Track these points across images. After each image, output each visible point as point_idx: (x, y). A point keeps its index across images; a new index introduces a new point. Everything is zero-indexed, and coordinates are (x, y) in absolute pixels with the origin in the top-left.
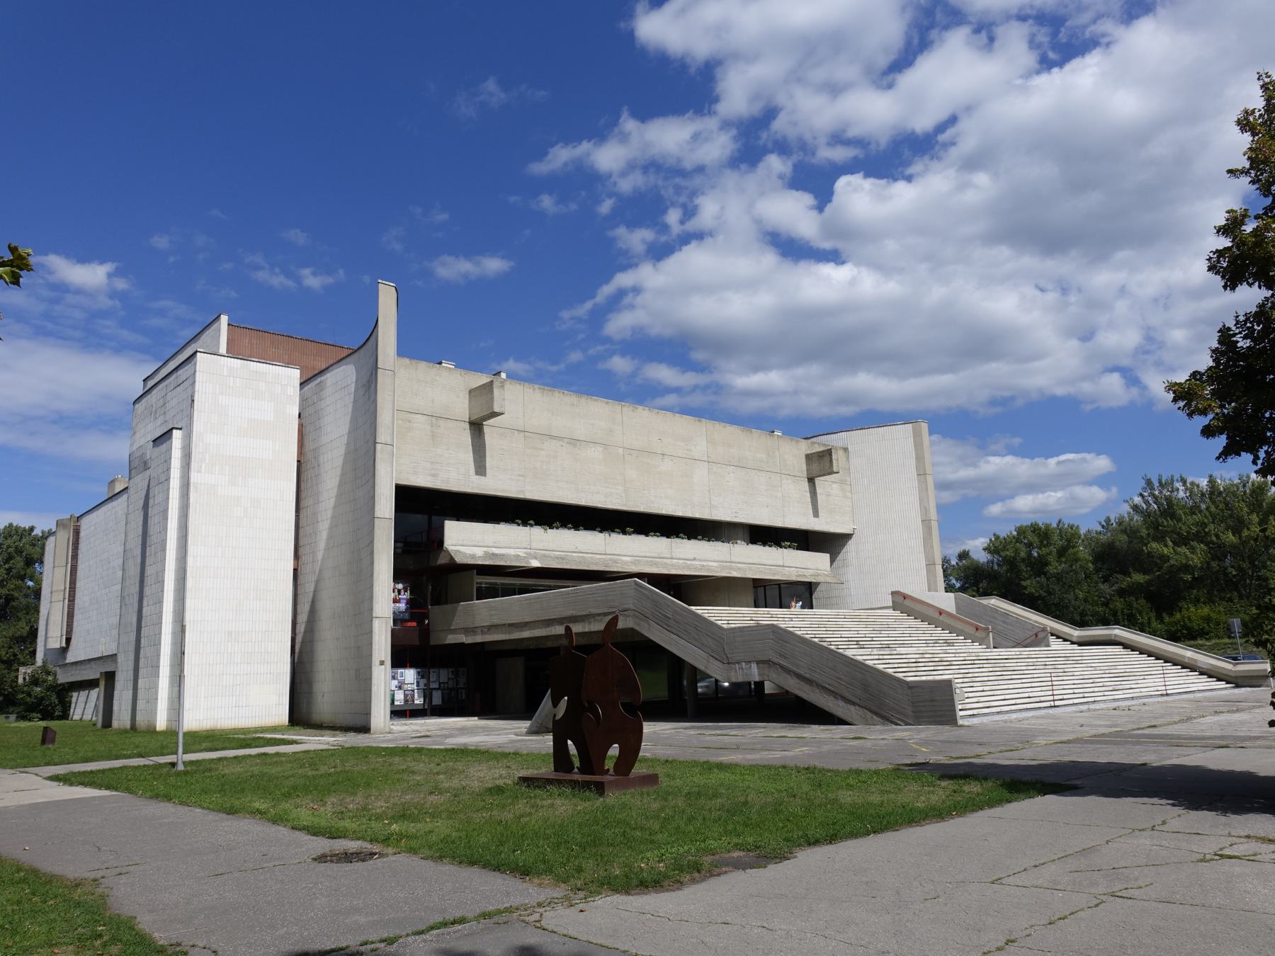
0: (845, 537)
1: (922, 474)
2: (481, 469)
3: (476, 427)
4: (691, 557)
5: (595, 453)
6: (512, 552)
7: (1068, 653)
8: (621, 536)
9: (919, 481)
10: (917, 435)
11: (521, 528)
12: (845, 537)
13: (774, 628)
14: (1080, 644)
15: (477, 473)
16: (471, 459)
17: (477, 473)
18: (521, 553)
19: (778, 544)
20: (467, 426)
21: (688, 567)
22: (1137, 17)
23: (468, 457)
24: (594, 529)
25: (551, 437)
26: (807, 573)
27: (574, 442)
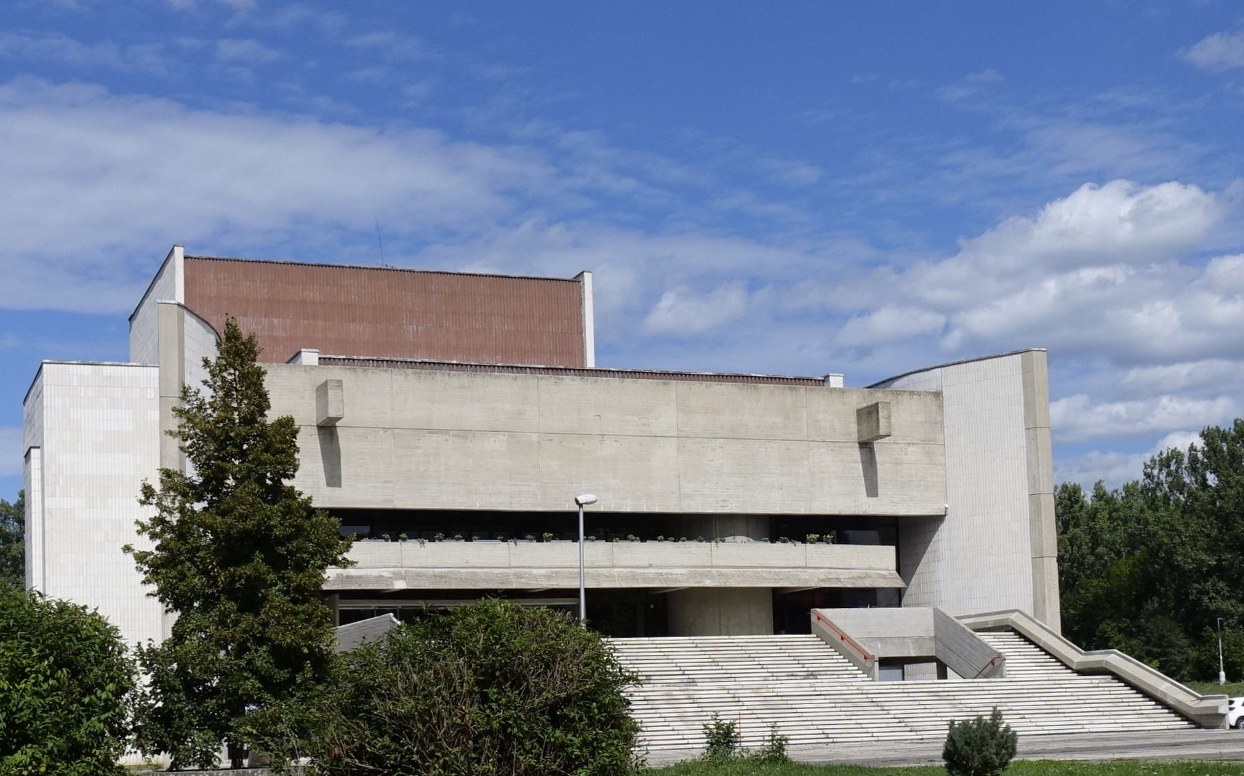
1: (1031, 428)
2: (872, 490)
3: (866, 446)
4: (646, 563)
5: (496, 444)
6: (375, 572)
7: (1066, 684)
8: (535, 544)
9: (1028, 438)
10: (1027, 371)
11: (390, 543)
13: (1087, 648)
14: (1081, 672)
15: (329, 485)
16: (322, 468)
17: (329, 485)
18: (386, 573)
19: (449, 535)
20: (315, 431)
21: (634, 578)
25: (431, 431)
27: (464, 434)
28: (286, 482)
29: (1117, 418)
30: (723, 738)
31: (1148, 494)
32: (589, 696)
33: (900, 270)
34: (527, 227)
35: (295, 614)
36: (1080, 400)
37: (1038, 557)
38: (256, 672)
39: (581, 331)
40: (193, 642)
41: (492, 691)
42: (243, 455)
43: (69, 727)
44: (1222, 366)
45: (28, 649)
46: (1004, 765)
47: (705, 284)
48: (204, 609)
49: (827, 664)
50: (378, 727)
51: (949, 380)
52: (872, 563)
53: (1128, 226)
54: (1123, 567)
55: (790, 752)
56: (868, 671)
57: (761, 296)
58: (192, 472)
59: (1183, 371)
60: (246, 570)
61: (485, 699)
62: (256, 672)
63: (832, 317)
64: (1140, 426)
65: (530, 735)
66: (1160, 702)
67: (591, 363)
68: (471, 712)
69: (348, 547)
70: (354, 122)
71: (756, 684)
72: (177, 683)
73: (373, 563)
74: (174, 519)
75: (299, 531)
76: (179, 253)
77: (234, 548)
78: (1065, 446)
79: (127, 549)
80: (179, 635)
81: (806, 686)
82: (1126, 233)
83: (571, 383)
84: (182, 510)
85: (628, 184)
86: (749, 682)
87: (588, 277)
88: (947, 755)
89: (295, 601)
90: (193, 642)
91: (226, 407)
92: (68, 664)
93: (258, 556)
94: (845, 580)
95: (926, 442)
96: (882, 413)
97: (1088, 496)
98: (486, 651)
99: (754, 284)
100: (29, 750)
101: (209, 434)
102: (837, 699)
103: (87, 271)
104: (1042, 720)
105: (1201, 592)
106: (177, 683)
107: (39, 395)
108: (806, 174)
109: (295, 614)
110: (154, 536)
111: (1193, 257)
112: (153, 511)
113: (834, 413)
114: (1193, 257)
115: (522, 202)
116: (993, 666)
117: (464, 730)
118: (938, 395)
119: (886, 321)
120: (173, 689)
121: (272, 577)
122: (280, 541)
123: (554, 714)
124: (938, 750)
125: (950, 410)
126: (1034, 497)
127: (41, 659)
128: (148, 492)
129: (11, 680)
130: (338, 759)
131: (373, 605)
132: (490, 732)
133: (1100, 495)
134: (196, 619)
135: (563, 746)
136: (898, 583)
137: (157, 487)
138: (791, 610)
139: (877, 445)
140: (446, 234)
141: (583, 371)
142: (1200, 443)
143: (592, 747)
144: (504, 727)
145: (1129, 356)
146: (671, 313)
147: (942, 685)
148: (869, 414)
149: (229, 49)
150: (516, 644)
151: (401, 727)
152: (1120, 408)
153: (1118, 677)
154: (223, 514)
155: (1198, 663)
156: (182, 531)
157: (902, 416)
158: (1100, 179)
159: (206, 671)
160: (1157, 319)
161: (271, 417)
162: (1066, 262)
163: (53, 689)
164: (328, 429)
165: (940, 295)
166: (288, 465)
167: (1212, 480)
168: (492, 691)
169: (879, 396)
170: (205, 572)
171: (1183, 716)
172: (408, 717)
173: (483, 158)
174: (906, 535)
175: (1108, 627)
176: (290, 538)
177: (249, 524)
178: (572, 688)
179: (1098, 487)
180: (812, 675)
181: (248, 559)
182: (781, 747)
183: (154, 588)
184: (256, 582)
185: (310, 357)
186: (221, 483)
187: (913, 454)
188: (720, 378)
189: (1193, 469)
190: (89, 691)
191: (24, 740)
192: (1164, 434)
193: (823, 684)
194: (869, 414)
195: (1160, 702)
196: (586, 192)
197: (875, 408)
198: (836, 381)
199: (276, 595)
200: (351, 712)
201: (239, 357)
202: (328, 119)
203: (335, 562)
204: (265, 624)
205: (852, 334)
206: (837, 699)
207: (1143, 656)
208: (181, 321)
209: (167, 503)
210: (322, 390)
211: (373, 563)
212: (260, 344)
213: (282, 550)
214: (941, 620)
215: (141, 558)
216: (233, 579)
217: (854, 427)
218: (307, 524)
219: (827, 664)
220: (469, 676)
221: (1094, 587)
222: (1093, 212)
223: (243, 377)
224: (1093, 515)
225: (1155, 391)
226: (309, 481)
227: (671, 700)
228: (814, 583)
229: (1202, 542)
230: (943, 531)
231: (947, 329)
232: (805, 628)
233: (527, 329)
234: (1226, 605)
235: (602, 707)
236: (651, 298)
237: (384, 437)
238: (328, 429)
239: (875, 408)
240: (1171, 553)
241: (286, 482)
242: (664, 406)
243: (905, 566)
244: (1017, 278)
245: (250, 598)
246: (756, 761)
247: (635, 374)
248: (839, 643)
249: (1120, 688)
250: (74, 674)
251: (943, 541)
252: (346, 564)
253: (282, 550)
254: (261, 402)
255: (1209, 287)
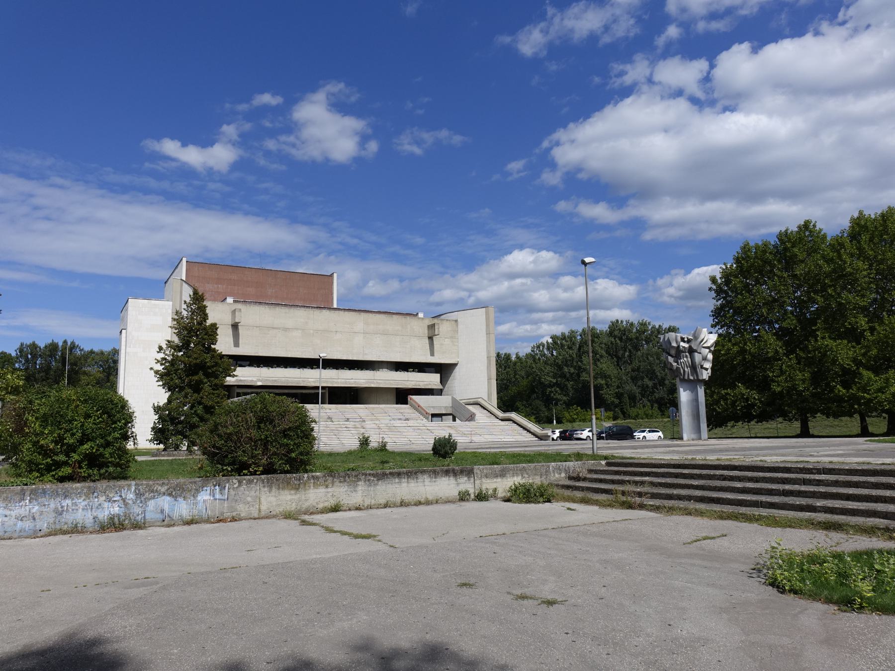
0: (455, 365)
1: (488, 334)
2: (432, 354)
3: (431, 338)
5: (297, 334)
10: (487, 314)
12: (455, 365)
13: (504, 412)
14: (502, 420)
18: (255, 379)
19: (278, 366)
22: (553, 160)
23: (231, 340)
24: (294, 367)
25: (274, 328)
26: (421, 384)
27: (286, 329)
28: (213, 346)
29: (527, 331)
30: (365, 442)
31: (531, 356)
32: (297, 428)
33: (453, 276)
34: (321, 256)
35: (213, 394)
36: (514, 324)
37: (489, 379)
38: (197, 415)
39: (332, 294)
40: (174, 404)
41: (262, 425)
42: (197, 336)
43: (106, 436)
44: (561, 314)
45: (92, 408)
46: (452, 453)
47: (384, 279)
48: (180, 392)
49: (413, 416)
50: (219, 436)
51: (461, 316)
52: (432, 380)
53: (532, 265)
54: (525, 382)
55: (388, 447)
56: (427, 418)
57: (405, 284)
58: (176, 340)
59: (550, 315)
60: (196, 378)
61: (259, 428)
62: (197, 415)
63: (430, 292)
64: (535, 334)
65: (276, 440)
66: (529, 431)
67: (335, 306)
68: (254, 433)
69: (235, 370)
70: (257, 215)
71: (388, 422)
72: (167, 419)
73: (245, 375)
74: (169, 358)
75: (216, 364)
76: (184, 260)
77: (192, 370)
78: (501, 339)
79: (151, 369)
80: (170, 401)
81: (404, 423)
82: (531, 267)
83: (326, 313)
84: (173, 355)
85: (355, 241)
86: (385, 421)
87: (335, 275)
88: (433, 449)
89: (214, 389)
90: (174, 404)
91: (192, 319)
92: (107, 413)
93: (201, 373)
94: (422, 386)
95: (452, 337)
96: (436, 327)
97: (513, 358)
98: (261, 411)
99: (401, 279)
100: (89, 444)
101: (185, 328)
102: (416, 428)
103: (153, 263)
104: (487, 437)
105: (551, 392)
106: (167, 419)
107: (127, 310)
108: (419, 240)
109: (213, 394)
110: (162, 364)
111: (555, 275)
112: (162, 355)
113: (419, 326)
114: (555, 275)
115: (317, 248)
116: (471, 418)
117: (251, 439)
118: (456, 321)
119: (448, 294)
120: (166, 421)
121: (206, 380)
122: (209, 367)
123: (285, 433)
124: (430, 447)
125: (460, 326)
126: (489, 358)
127: (97, 411)
128: (160, 348)
129: (85, 418)
130: (206, 448)
131: (249, 391)
132: (261, 440)
133: (518, 357)
134: (176, 395)
135: (287, 445)
136: (441, 387)
137: (164, 347)
138: (402, 396)
139: (434, 338)
140: (289, 256)
141: (331, 309)
142: (550, 341)
143: (298, 445)
144: (267, 437)
145: (532, 309)
146: (373, 288)
147: (454, 424)
148: (432, 327)
149: (212, 186)
150: (271, 409)
151: (229, 437)
152: (528, 327)
153: (515, 422)
154: (188, 357)
155: (547, 417)
156: (172, 363)
157: (443, 328)
158: (521, 247)
159: (179, 414)
160: (541, 296)
161: (209, 322)
162: (512, 276)
163: (101, 422)
164: (235, 326)
165: (470, 286)
166: (214, 341)
167: (555, 353)
168: (262, 425)
169: (435, 321)
170: (180, 378)
171: (536, 436)
172: (230, 434)
173: (304, 230)
174: (444, 370)
175: (518, 404)
176: (213, 367)
177: (198, 361)
178: (291, 425)
179: (517, 354)
180: (407, 419)
181: (197, 373)
182: (385, 446)
183: (161, 383)
184: (200, 382)
185: (230, 300)
186: (189, 345)
187: (447, 341)
188: (379, 312)
189: (548, 349)
190: (115, 423)
191: (89, 440)
192: (543, 337)
193: (410, 423)
194: (432, 327)
195: (529, 431)
196: (340, 243)
197: (434, 325)
198: (421, 315)
199: (207, 387)
200: (211, 432)
201: (198, 298)
202: (246, 213)
203: (230, 376)
204: (202, 398)
205: (435, 298)
206: (416, 428)
207: (527, 416)
208: (182, 286)
209: (168, 352)
210: (234, 312)
211: (245, 375)
212: (207, 296)
213: (210, 371)
214: (454, 400)
215: (156, 372)
216: (190, 381)
217: (426, 331)
218: (220, 361)
219: (413, 416)
220: (254, 420)
221: (514, 390)
222: (521, 259)
223: (199, 308)
224: (515, 364)
225: (542, 321)
226: (224, 345)
227: (355, 427)
228: (410, 387)
229: (551, 374)
230: (457, 369)
231: (470, 296)
232: (406, 403)
233: (313, 293)
234: (559, 397)
235: (302, 431)
236: (365, 282)
237: (253, 330)
238: (235, 326)
239: (434, 325)
240: (540, 378)
241: (213, 346)
242: (359, 322)
243: (443, 381)
244: (494, 281)
245: (197, 388)
246: (376, 450)
247: (349, 310)
248: (417, 408)
249: (515, 426)
250: (109, 416)
251: (457, 372)
252: (234, 376)
253: (210, 371)
254: (205, 317)
255: (559, 286)
